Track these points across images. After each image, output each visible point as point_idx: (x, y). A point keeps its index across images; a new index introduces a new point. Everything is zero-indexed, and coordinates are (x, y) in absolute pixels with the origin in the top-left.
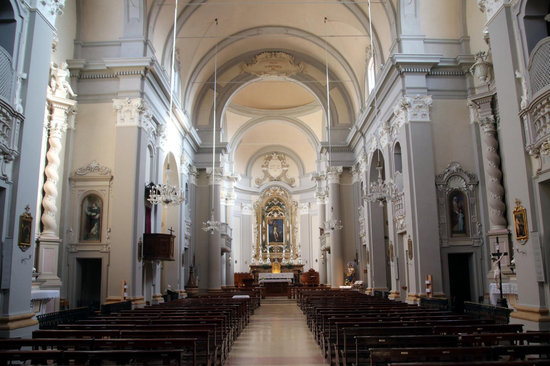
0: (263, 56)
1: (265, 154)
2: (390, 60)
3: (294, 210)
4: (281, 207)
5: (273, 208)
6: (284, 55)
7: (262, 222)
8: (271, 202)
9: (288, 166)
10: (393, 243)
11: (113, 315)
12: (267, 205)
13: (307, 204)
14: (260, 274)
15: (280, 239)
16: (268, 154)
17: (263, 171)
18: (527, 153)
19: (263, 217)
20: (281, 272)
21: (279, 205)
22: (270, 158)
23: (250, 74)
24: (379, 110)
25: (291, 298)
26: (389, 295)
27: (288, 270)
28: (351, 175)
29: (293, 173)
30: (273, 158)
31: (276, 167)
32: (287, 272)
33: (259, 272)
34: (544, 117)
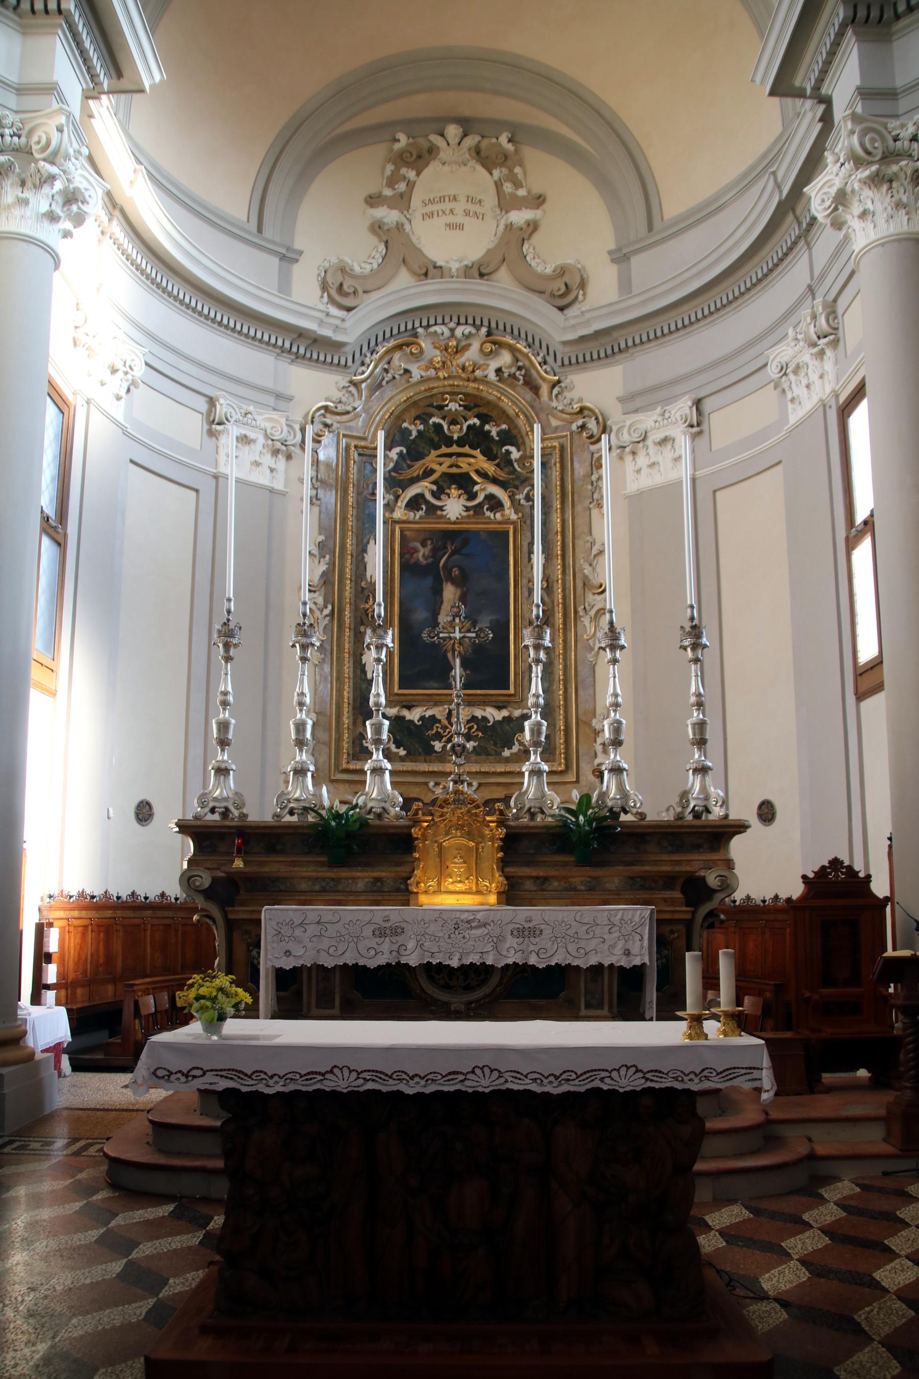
1: (383, 131)
3: (580, 469)
4: (490, 455)
5: (437, 462)
8: (423, 418)
9: (539, 200)
13: (683, 407)
14: (271, 916)
15: (491, 668)
16: (409, 124)
17: (377, 228)
20: (511, 895)
21: (477, 439)
22: (420, 157)
27: (579, 876)
29: (577, 231)
30: (445, 153)
31: (460, 207)
32: (572, 896)
33: (276, 890)
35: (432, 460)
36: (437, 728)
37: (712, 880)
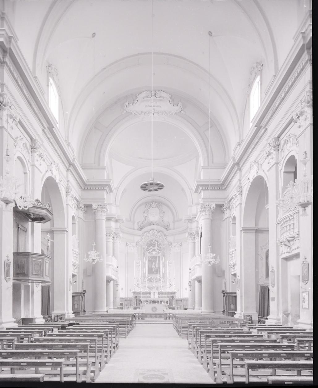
0: (144, 95)
2: (301, 36)
6: (164, 94)
7: (144, 258)
10: (275, 269)
11: (29, 325)
12: (147, 244)
18: (277, 244)
19: (144, 254)
23: (131, 113)
24: (266, 129)
25: (166, 319)
26: (235, 315)
28: (223, 212)
34: (286, 227)
35: (151, 247)
36: (152, 279)
37: (174, 296)
